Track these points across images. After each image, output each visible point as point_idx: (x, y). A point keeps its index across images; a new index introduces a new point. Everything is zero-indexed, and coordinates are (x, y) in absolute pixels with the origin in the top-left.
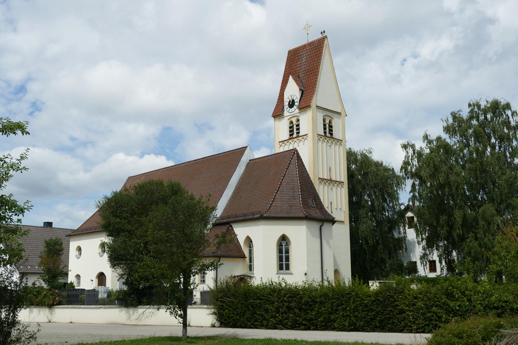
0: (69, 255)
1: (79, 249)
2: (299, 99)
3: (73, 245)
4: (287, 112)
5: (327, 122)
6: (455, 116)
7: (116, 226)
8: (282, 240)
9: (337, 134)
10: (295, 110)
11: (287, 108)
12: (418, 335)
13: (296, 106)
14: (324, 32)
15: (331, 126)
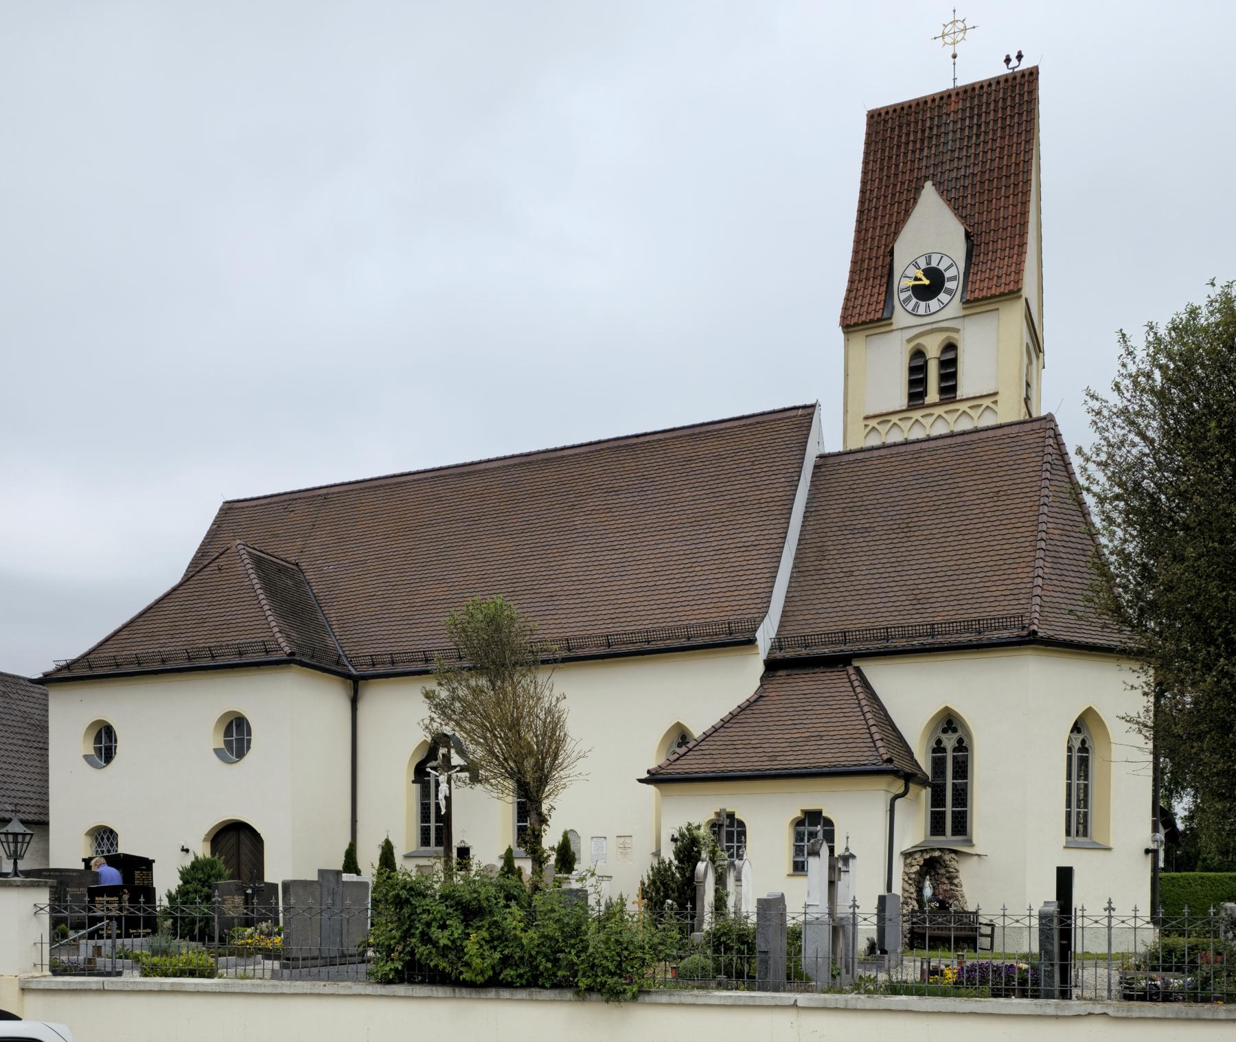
1: (104, 743)
2: (962, 265)
3: (69, 721)
5: (933, 349)
7: (871, 722)
8: (945, 731)
9: (966, 387)
10: (947, 306)
11: (908, 300)
13: (949, 292)
14: (1020, 57)
15: (949, 367)
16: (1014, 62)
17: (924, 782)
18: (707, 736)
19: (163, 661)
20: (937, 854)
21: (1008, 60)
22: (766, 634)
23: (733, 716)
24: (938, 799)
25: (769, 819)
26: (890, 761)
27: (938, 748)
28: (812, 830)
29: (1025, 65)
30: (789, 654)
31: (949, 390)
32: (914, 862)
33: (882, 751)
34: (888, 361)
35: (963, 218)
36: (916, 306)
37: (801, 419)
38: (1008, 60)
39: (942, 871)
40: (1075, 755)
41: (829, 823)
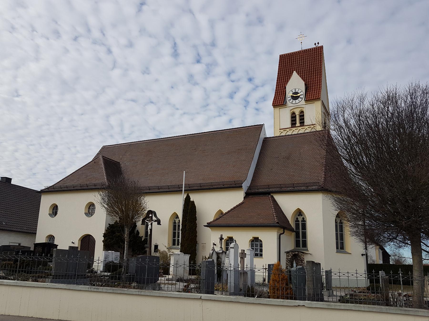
0: (38, 221)
1: (54, 210)
3: (46, 202)
4: (290, 102)
5: (297, 113)
6: (10, 179)
8: (299, 215)
10: (301, 102)
11: (290, 100)
12: (383, 307)
14: (318, 43)
16: (317, 45)
17: (291, 230)
18: (226, 213)
19: (81, 187)
20: (296, 253)
21: (315, 44)
22: (246, 185)
23: (234, 208)
24: (297, 236)
25: (243, 239)
26: (278, 223)
27: (297, 221)
28: (256, 243)
29: (319, 45)
30: (253, 191)
31: (302, 123)
32: (289, 255)
33: (276, 220)
34: (285, 116)
35: (304, 80)
36: (293, 101)
37: (259, 128)
38: (315, 44)
39: (299, 258)
40: (338, 225)
41: (261, 241)
